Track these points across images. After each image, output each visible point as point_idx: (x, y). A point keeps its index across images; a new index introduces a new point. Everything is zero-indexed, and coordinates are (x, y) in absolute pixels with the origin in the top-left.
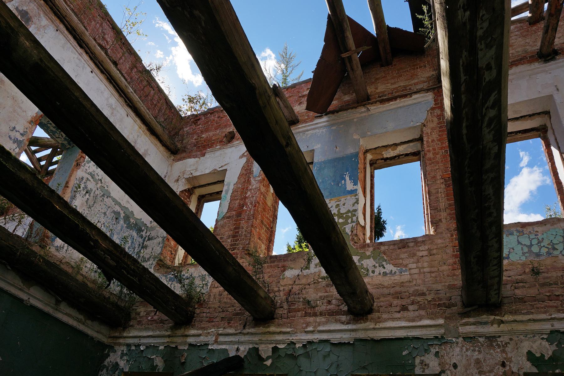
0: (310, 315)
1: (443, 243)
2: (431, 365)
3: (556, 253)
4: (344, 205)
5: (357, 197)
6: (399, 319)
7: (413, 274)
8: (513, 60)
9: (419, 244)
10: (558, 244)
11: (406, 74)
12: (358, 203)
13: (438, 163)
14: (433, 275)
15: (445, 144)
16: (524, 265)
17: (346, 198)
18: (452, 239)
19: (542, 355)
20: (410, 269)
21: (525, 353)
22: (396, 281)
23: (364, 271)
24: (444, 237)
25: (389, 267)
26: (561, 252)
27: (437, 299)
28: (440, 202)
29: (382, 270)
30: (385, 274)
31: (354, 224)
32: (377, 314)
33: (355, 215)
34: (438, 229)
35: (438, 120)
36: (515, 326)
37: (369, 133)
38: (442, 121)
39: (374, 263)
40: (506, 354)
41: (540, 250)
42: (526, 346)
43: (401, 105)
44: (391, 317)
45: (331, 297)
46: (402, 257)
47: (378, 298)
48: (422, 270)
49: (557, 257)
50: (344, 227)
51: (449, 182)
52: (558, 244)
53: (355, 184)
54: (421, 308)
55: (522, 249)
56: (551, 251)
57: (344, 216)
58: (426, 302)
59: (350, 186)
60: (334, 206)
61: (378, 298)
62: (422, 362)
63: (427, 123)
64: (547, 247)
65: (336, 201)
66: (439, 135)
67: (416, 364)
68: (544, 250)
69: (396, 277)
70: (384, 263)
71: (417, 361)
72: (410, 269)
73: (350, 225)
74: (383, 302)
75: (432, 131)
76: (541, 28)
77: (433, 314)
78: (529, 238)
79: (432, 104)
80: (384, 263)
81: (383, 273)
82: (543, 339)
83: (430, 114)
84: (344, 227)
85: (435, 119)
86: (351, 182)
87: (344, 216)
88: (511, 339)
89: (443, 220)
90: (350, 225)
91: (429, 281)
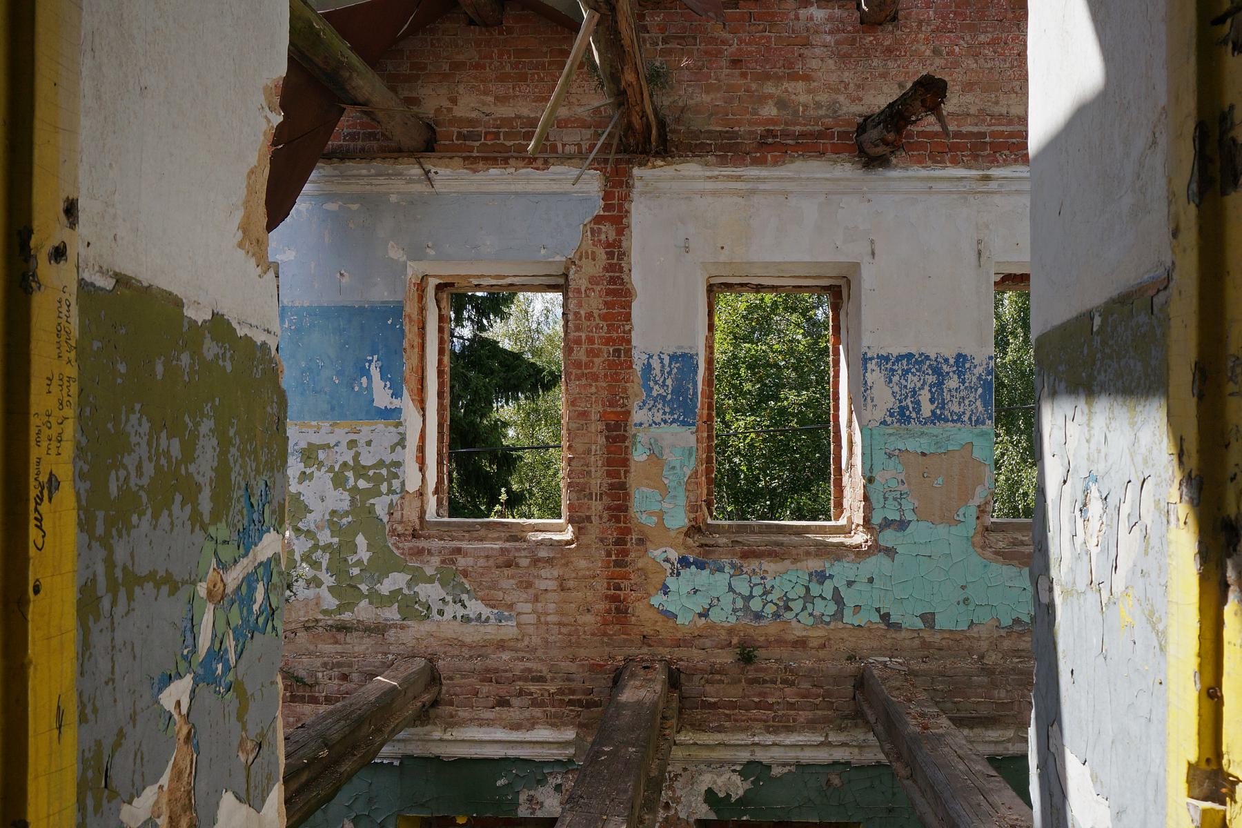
0: (302, 700)
1: (588, 569)
2: (546, 804)
3: (788, 615)
4: (369, 443)
5: (401, 429)
6: (489, 723)
7: (525, 624)
8: (805, 129)
9: (540, 564)
10: (796, 600)
11: (539, 76)
12: (404, 447)
13: (595, 378)
14: (564, 630)
15: (617, 332)
16: (731, 631)
17: (373, 428)
18: (609, 562)
19: (728, 796)
20: (519, 614)
21: (703, 792)
22: (489, 637)
23: (421, 609)
24: (592, 557)
25: (475, 607)
26: (797, 615)
27: (567, 691)
28: (591, 477)
29: (461, 612)
30: (466, 619)
31: (395, 498)
32: (447, 707)
33: (396, 476)
34: (583, 537)
35: (608, 259)
36: (695, 752)
37: (432, 252)
38: (616, 264)
39: (443, 594)
40: (674, 791)
41: (764, 606)
42: (706, 780)
43: (519, 187)
44: (476, 717)
45: (349, 667)
46: (504, 586)
47: (451, 678)
48: (542, 619)
49: (788, 622)
50: (372, 501)
51: (615, 433)
52: (796, 600)
53: (397, 394)
54: (535, 703)
55: (734, 602)
56: (782, 611)
57: (371, 473)
58: (546, 694)
59: (382, 397)
60: (344, 444)
61: (451, 678)
62: (531, 799)
63: (580, 259)
64: (775, 604)
65: (347, 430)
66: (606, 303)
67: (521, 801)
68: (770, 609)
69: (489, 629)
70: (465, 597)
71: (523, 798)
72: (519, 614)
73: (387, 499)
74: (461, 687)
75: (590, 286)
76: (882, 45)
77: (557, 718)
78: (750, 581)
79: (598, 208)
80: (465, 597)
81: (462, 617)
82: (734, 771)
83: (589, 233)
84: (372, 501)
85: (601, 253)
86: (385, 386)
87: (371, 473)
88: (685, 769)
89: (593, 518)
90: (387, 499)
91: (555, 642)
